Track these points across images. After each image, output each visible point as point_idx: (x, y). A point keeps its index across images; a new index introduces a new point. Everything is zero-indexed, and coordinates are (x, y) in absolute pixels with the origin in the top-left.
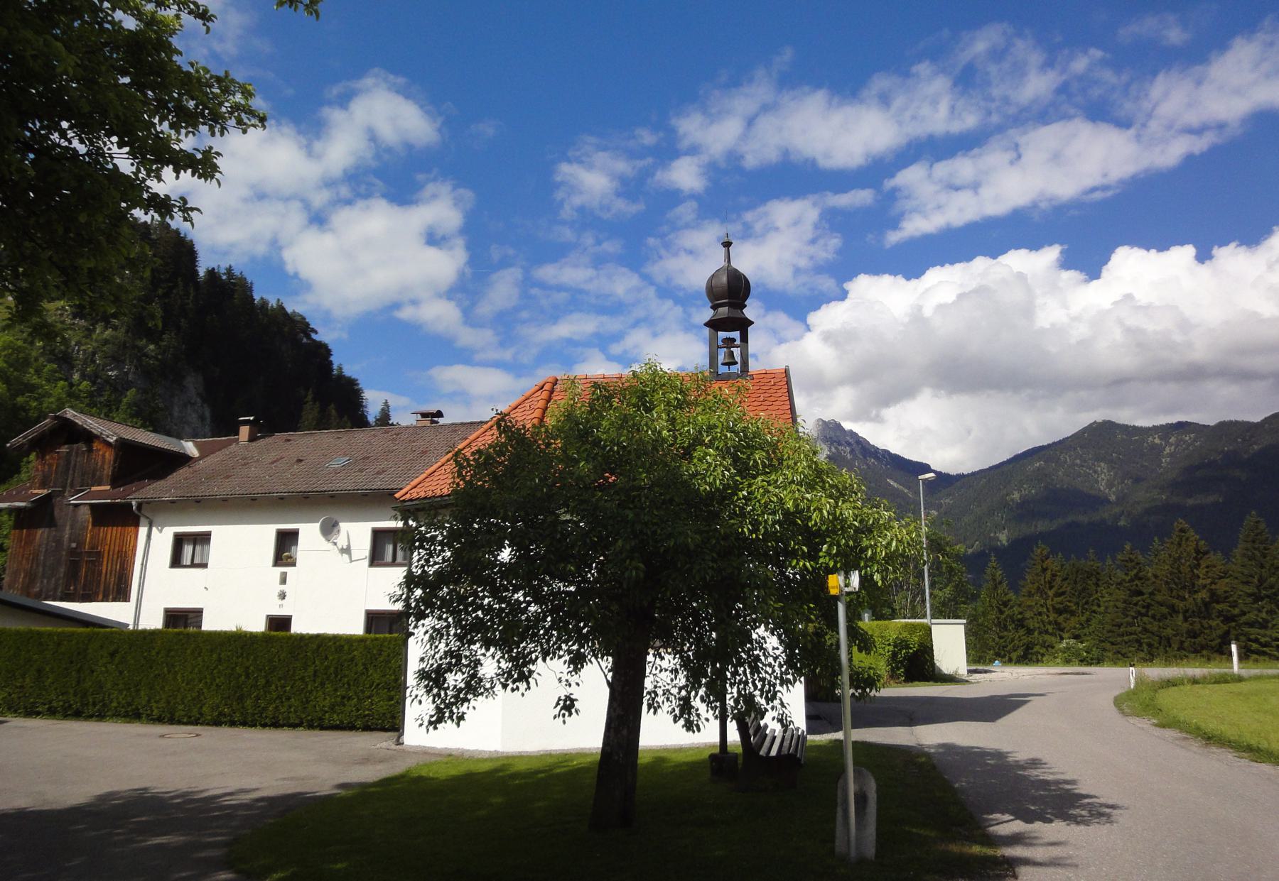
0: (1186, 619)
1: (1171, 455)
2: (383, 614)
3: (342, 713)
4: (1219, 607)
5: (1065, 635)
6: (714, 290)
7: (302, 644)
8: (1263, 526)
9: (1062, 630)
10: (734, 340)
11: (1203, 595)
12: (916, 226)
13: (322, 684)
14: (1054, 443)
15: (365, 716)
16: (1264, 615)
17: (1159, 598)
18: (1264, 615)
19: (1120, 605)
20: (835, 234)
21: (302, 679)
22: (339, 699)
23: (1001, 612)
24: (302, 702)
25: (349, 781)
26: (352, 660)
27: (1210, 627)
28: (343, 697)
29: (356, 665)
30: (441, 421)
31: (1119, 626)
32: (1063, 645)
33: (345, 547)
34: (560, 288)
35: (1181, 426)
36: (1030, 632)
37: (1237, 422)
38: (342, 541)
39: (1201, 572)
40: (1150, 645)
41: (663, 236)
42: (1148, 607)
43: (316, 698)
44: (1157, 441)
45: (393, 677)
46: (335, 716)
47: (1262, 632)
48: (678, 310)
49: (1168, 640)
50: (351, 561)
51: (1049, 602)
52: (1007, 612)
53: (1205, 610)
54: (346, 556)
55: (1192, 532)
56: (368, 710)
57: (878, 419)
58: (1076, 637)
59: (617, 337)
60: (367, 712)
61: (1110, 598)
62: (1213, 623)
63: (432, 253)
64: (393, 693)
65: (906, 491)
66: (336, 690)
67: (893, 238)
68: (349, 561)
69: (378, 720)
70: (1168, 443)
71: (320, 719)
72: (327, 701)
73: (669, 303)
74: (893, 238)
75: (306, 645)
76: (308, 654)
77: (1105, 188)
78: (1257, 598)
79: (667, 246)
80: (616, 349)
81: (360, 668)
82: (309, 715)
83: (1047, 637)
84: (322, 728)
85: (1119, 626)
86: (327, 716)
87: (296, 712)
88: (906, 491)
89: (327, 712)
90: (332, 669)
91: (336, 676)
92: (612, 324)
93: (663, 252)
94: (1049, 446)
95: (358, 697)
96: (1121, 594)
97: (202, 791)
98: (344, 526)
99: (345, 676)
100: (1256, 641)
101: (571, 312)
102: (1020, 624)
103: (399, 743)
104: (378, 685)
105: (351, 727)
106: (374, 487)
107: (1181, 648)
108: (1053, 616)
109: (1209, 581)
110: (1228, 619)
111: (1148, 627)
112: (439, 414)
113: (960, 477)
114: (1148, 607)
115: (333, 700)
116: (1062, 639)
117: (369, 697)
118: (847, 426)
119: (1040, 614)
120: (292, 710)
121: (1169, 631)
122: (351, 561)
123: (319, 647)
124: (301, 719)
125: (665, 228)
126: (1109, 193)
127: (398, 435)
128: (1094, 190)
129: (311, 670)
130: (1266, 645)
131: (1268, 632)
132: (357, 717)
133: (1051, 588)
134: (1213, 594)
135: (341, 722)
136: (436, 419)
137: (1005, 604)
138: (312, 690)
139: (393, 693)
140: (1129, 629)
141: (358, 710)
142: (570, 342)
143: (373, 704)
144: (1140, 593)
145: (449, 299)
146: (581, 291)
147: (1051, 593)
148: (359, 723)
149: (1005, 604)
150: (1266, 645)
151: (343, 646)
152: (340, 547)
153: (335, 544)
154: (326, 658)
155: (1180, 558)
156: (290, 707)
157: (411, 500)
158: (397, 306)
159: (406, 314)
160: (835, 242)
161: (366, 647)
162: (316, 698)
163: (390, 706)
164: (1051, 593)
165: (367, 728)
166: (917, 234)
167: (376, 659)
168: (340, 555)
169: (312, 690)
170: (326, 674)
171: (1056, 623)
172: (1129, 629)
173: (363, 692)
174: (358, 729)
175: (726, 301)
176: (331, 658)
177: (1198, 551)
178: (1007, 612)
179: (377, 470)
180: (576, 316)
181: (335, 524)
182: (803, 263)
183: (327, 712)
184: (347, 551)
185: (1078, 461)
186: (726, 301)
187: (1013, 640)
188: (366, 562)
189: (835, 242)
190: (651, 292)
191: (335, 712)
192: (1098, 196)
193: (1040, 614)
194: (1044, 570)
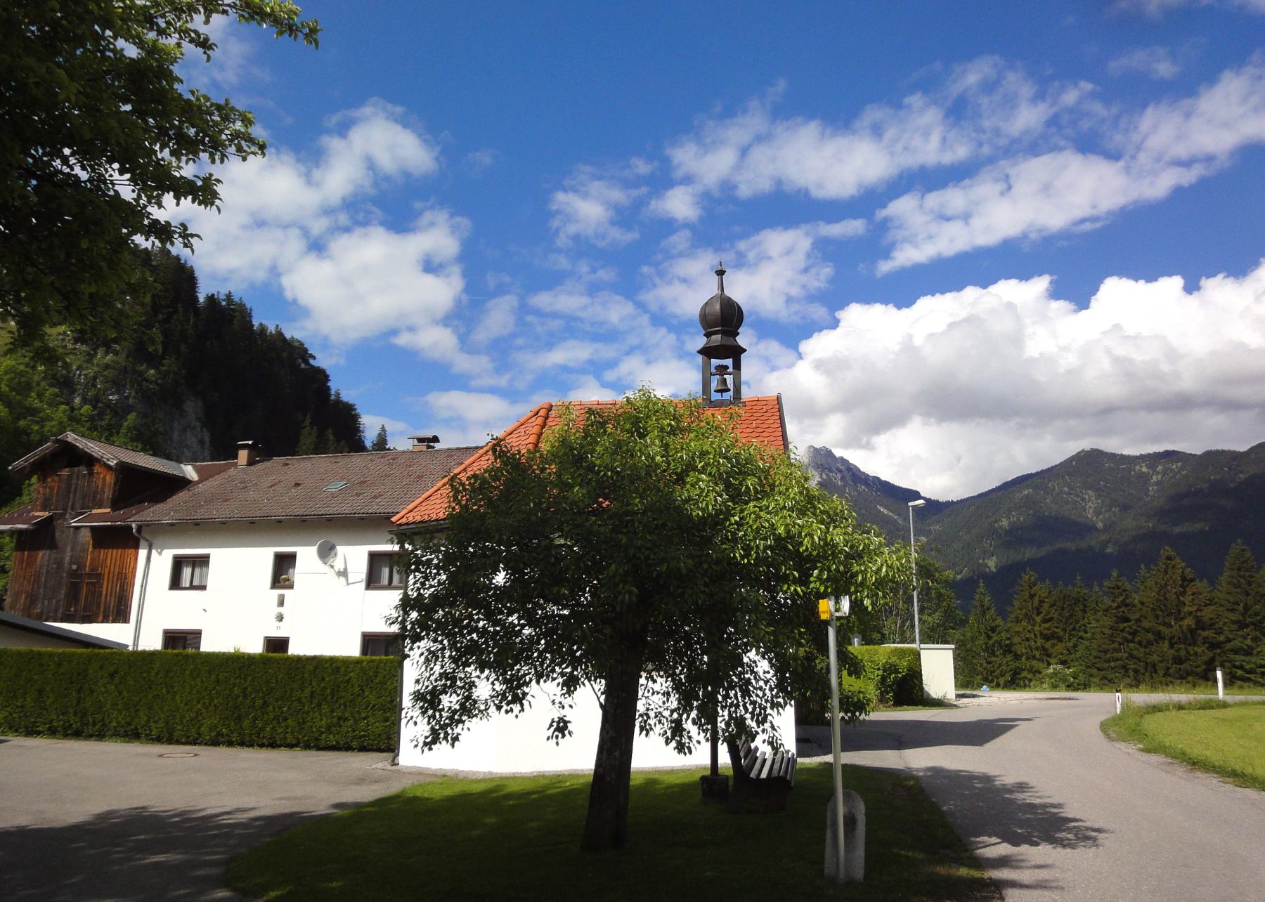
0: (1171, 646)
1: (1158, 483)
5: (1051, 661)
7: (300, 665)
8: (1248, 554)
9: (1049, 656)
10: (727, 367)
12: (907, 256)
13: (319, 705)
15: (361, 737)
16: (1249, 642)
17: (1146, 624)
18: (1249, 642)
19: (1107, 631)
21: (299, 700)
23: (989, 638)
26: (348, 682)
27: (1196, 653)
28: (339, 718)
30: (438, 446)
31: (1106, 652)
33: (342, 570)
34: (554, 315)
35: (1168, 455)
36: (1017, 657)
37: (1223, 451)
38: (339, 564)
39: (1187, 599)
40: (1136, 671)
44: (1144, 469)
47: (1247, 658)
48: (672, 338)
49: (1154, 666)
50: (348, 584)
51: (1037, 628)
52: (995, 638)
53: (1190, 637)
54: (342, 579)
56: (364, 731)
57: (868, 447)
58: (1063, 663)
59: (612, 364)
60: (363, 733)
61: (1097, 624)
62: (1199, 650)
63: (430, 280)
64: (388, 714)
66: (332, 711)
67: (885, 267)
71: (317, 739)
73: (663, 331)
74: (885, 267)
75: (304, 667)
77: (1094, 219)
79: (661, 274)
82: (305, 736)
83: (1034, 663)
84: (319, 748)
85: (1106, 652)
86: (324, 736)
87: (292, 733)
90: (328, 691)
91: (333, 697)
92: (607, 352)
93: (657, 280)
94: (1037, 474)
96: (1108, 621)
99: (341, 698)
102: (1008, 649)
103: (394, 763)
104: (374, 706)
105: (348, 748)
108: (1040, 642)
109: (1195, 608)
110: (1213, 646)
111: (1135, 653)
112: (436, 439)
115: (329, 721)
116: (1049, 664)
118: (838, 452)
119: (1028, 640)
120: (289, 730)
121: (1155, 658)
122: (348, 584)
124: (298, 739)
125: (659, 257)
126: (1098, 225)
127: (394, 459)
128: (1083, 221)
129: (307, 691)
131: (1253, 659)
133: (1038, 614)
134: (1198, 621)
135: (338, 742)
136: (432, 444)
139: (388, 714)
140: (1115, 655)
142: (565, 369)
144: (1127, 620)
145: (446, 325)
146: (577, 319)
147: (1038, 619)
148: (354, 744)
149: (993, 630)
152: (337, 570)
153: (332, 567)
155: (1166, 585)
158: (394, 332)
159: (403, 340)
160: (827, 271)
161: (362, 669)
163: (386, 727)
164: (1038, 619)
165: (363, 749)
166: (908, 264)
170: (322, 695)
172: (1115, 655)
173: (359, 713)
176: (327, 679)
177: (1184, 579)
178: (995, 638)
179: (374, 494)
180: (571, 343)
181: (332, 548)
182: (795, 291)
184: (343, 573)
185: (1066, 489)
187: (1000, 665)
188: (363, 585)
189: (827, 271)
190: (645, 320)
192: (1088, 227)
194: (1032, 596)
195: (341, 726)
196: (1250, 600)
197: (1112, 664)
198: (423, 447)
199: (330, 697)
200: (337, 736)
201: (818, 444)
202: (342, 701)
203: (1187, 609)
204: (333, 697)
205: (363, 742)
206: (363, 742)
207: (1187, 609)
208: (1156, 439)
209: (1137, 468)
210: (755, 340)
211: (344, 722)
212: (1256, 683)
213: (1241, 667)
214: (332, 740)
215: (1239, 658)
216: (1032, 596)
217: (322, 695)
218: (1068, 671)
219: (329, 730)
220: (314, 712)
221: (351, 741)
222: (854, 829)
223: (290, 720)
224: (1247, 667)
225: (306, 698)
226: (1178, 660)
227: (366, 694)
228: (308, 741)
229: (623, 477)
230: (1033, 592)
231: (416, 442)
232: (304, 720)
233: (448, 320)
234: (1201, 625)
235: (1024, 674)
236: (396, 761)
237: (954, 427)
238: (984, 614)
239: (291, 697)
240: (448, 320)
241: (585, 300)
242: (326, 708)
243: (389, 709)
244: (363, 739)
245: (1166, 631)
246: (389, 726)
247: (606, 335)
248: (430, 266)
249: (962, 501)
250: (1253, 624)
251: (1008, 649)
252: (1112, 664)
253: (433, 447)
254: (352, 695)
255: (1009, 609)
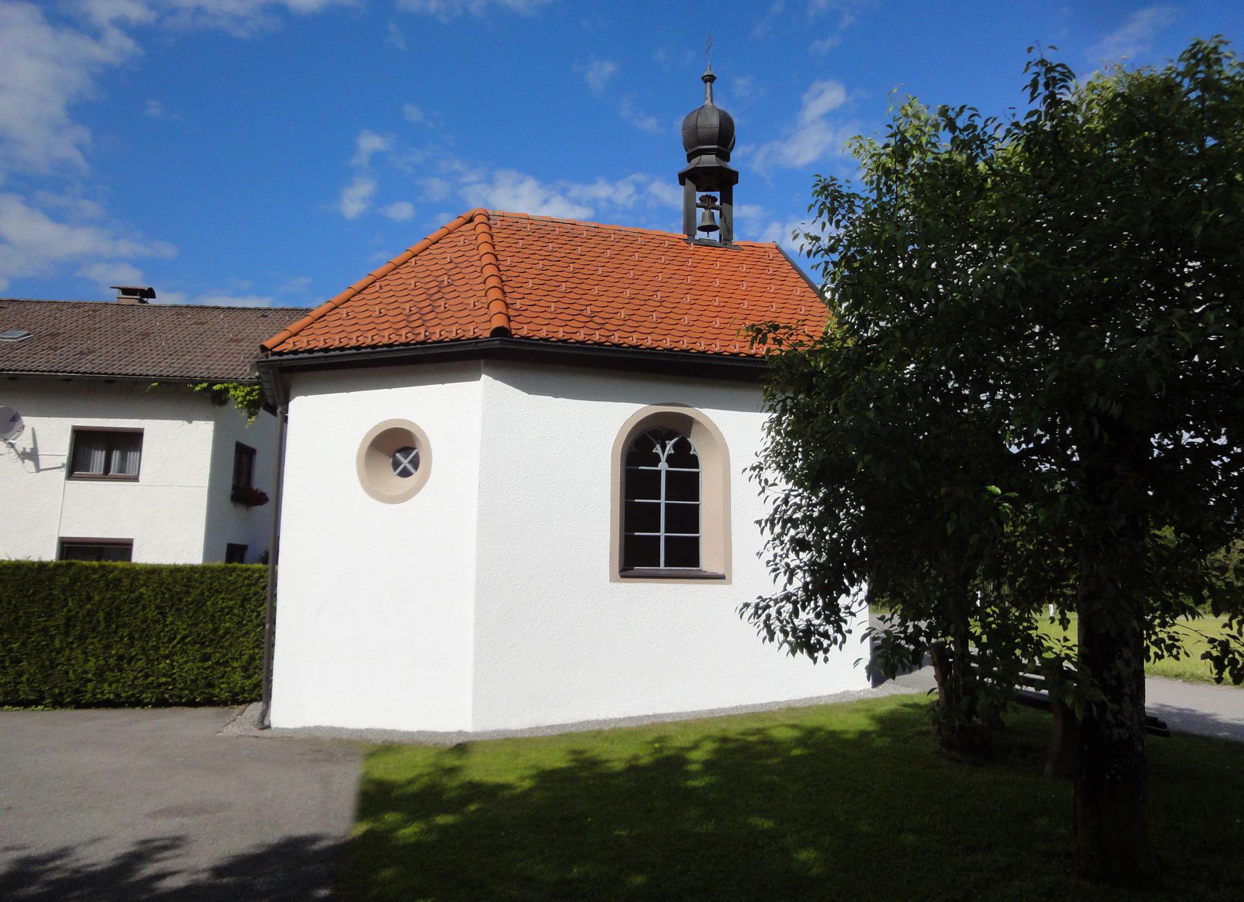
2: (99, 544)
3: (117, 681)
6: (699, 130)
7: (42, 576)
10: (715, 199)
13: (82, 638)
15: (159, 686)
21: (45, 630)
22: (112, 661)
24: (42, 666)
26: (137, 601)
28: (121, 658)
29: (144, 608)
30: (151, 301)
33: (28, 450)
38: (23, 442)
43: (69, 660)
45: (210, 626)
46: (106, 686)
50: (38, 470)
54: (29, 464)
56: (165, 675)
60: (164, 680)
64: (208, 650)
66: (107, 647)
68: (33, 469)
69: (182, 689)
71: (77, 691)
72: (91, 664)
75: (51, 579)
76: (55, 592)
81: (152, 613)
82: (55, 687)
84: (79, 705)
86: (90, 686)
87: (29, 682)
89: (90, 681)
90: (101, 615)
91: (108, 626)
95: (147, 657)
97: (94, 865)
98: (28, 421)
99: (125, 625)
103: (263, 724)
104: (184, 637)
105: (136, 703)
106: (82, 370)
112: (150, 293)
115: (102, 662)
117: (166, 657)
120: (24, 678)
122: (38, 470)
123: (75, 580)
124: (42, 692)
127: (95, 311)
129: (60, 618)
132: (147, 687)
135: (118, 696)
136: (145, 299)
138: (62, 649)
139: (208, 650)
141: (147, 676)
143: (173, 667)
148: (147, 696)
151: (120, 580)
152: (20, 450)
153: (12, 446)
154: (90, 598)
156: (20, 675)
157: (295, 352)
161: (161, 582)
162: (69, 660)
163: (206, 669)
165: (161, 703)
167: (180, 600)
168: (20, 461)
169: (62, 649)
170: (89, 622)
173: (156, 648)
174: (147, 704)
175: (716, 147)
176: (97, 598)
179: (78, 350)
181: (15, 418)
183: (90, 681)
184: (32, 455)
186: (716, 147)
188: (63, 473)
191: (105, 680)
195: (121, 670)
198: (133, 300)
199: (103, 625)
200: (114, 686)
202: (126, 631)
204: (108, 626)
205: (163, 693)
206: (163, 693)
211: (129, 663)
214: (108, 691)
217: (89, 622)
219: (101, 676)
220: (72, 649)
221: (142, 692)
223: (25, 663)
225: (57, 627)
227: (169, 620)
228: (61, 694)
229: (974, 257)
231: (119, 293)
232: (52, 662)
236: (266, 723)
239: (27, 625)
242: (94, 644)
243: (212, 641)
244: (163, 688)
246: (209, 667)
250: (38, 631)
253: (146, 302)
254: (144, 621)
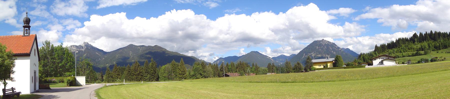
0: (136, 76)
1: (141, 50)
4: (140, 74)
5: (118, 79)
8: (148, 62)
9: (118, 78)
11: (139, 72)
12: (102, 6)
14: (124, 48)
16: (147, 75)
17: (132, 73)
18: (147, 75)
19: (127, 74)
20: (87, 6)
23: (109, 75)
25: (118, 48)
27: (139, 77)
31: (126, 77)
32: (118, 80)
34: (34, 16)
35: (143, 46)
36: (113, 78)
37: (150, 46)
39: (139, 68)
40: (130, 80)
41: (53, 5)
42: (131, 74)
44: (139, 48)
47: (146, 77)
48: (57, 20)
49: (133, 79)
51: (116, 73)
52: (110, 75)
53: (139, 75)
55: (138, 62)
57: (94, 42)
58: (120, 79)
59: (46, 26)
61: (125, 72)
62: (139, 76)
63: (11, 10)
65: (99, 55)
67: (98, 8)
70: (141, 48)
73: (55, 19)
74: (98, 8)
77: (135, 3)
78: (146, 72)
79: (55, 7)
80: (46, 28)
83: (116, 79)
85: (126, 77)
88: (99, 55)
92: (45, 23)
93: (54, 8)
94: (123, 48)
96: (127, 72)
100: (145, 79)
101: (37, 21)
102: (112, 77)
107: (135, 80)
108: (117, 76)
109: (139, 70)
110: (142, 76)
111: (130, 77)
113: (108, 52)
114: (131, 74)
116: (118, 79)
118: (89, 43)
119: (115, 75)
121: (133, 78)
125: (54, 4)
126: (135, 5)
128: (133, 3)
130: (146, 79)
131: (147, 77)
133: (117, 71)
134: (140, 72)
137: (109, 74)
140: (128, 77)
142: (37, 27)
144: (130, 72)
145: (14, 19)
146: (39, 17)
147: (117, 72)
149: (109, 74)
150: (146, 79)
155: (136, 66)
158: (5, 20)
159: (7, 22)
160: (87, 7)
164: (117, 72)
166: (102, 7)
171: (117, 77)
172: (128, 77)
177: (138, 65)
178: (110, 75)
180: (38, 21)
182: (82, 11)
185: (127, 51)
187: (110, 79)
189: (87, 7)
190: (52, 16)
192: (134, 4)
193: (115, 75)
194: (116, 68)
196: (147, 69)
197: (127, 79)
201: (86, 41)
203: (138, 70)
207: (138, 70)
208: (141, 43)
209: (138, 48)
210: (73, 20)
212: (146, 81)
213: (145, 79)
215: (145, 77)
216: (116, 68)
218: (120, 80)
222: (80, 88)
224: (146, 79)
226: (136, 78)
230: (116, 67)
233: (14, 17)
234: (140, 73)
235: (114, 81)
237: (110, 39)
238: (108, 71)
240: (14, 17)
241: (40, 13)
245: (135, 74)
247: (44, 20)
248: (10, 7)
249: (110, 52)
251: (112, 77)
252: (127, 79)
255: (112, 70)
